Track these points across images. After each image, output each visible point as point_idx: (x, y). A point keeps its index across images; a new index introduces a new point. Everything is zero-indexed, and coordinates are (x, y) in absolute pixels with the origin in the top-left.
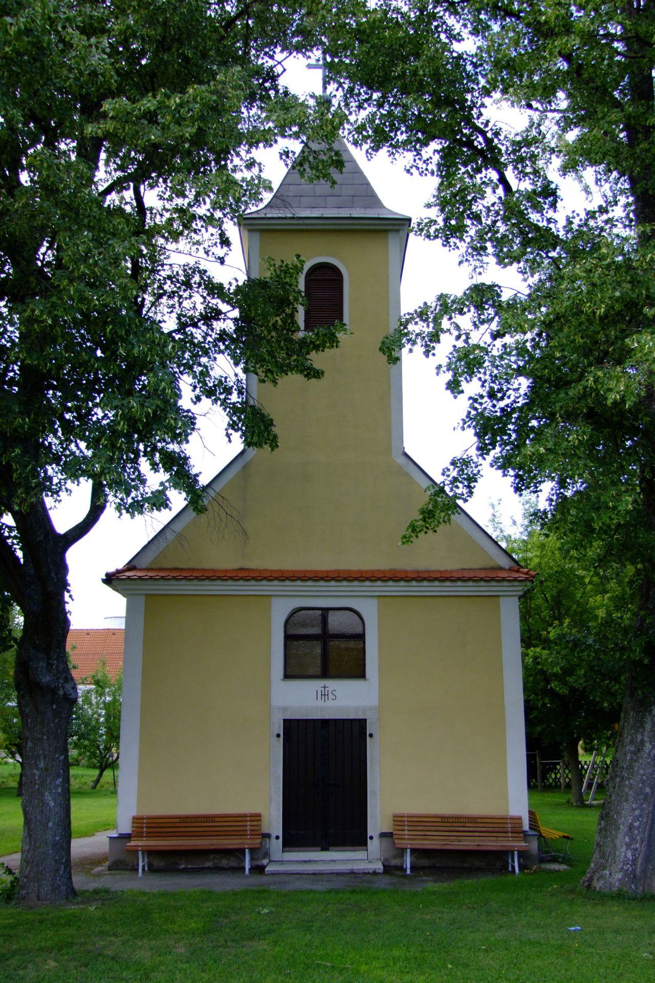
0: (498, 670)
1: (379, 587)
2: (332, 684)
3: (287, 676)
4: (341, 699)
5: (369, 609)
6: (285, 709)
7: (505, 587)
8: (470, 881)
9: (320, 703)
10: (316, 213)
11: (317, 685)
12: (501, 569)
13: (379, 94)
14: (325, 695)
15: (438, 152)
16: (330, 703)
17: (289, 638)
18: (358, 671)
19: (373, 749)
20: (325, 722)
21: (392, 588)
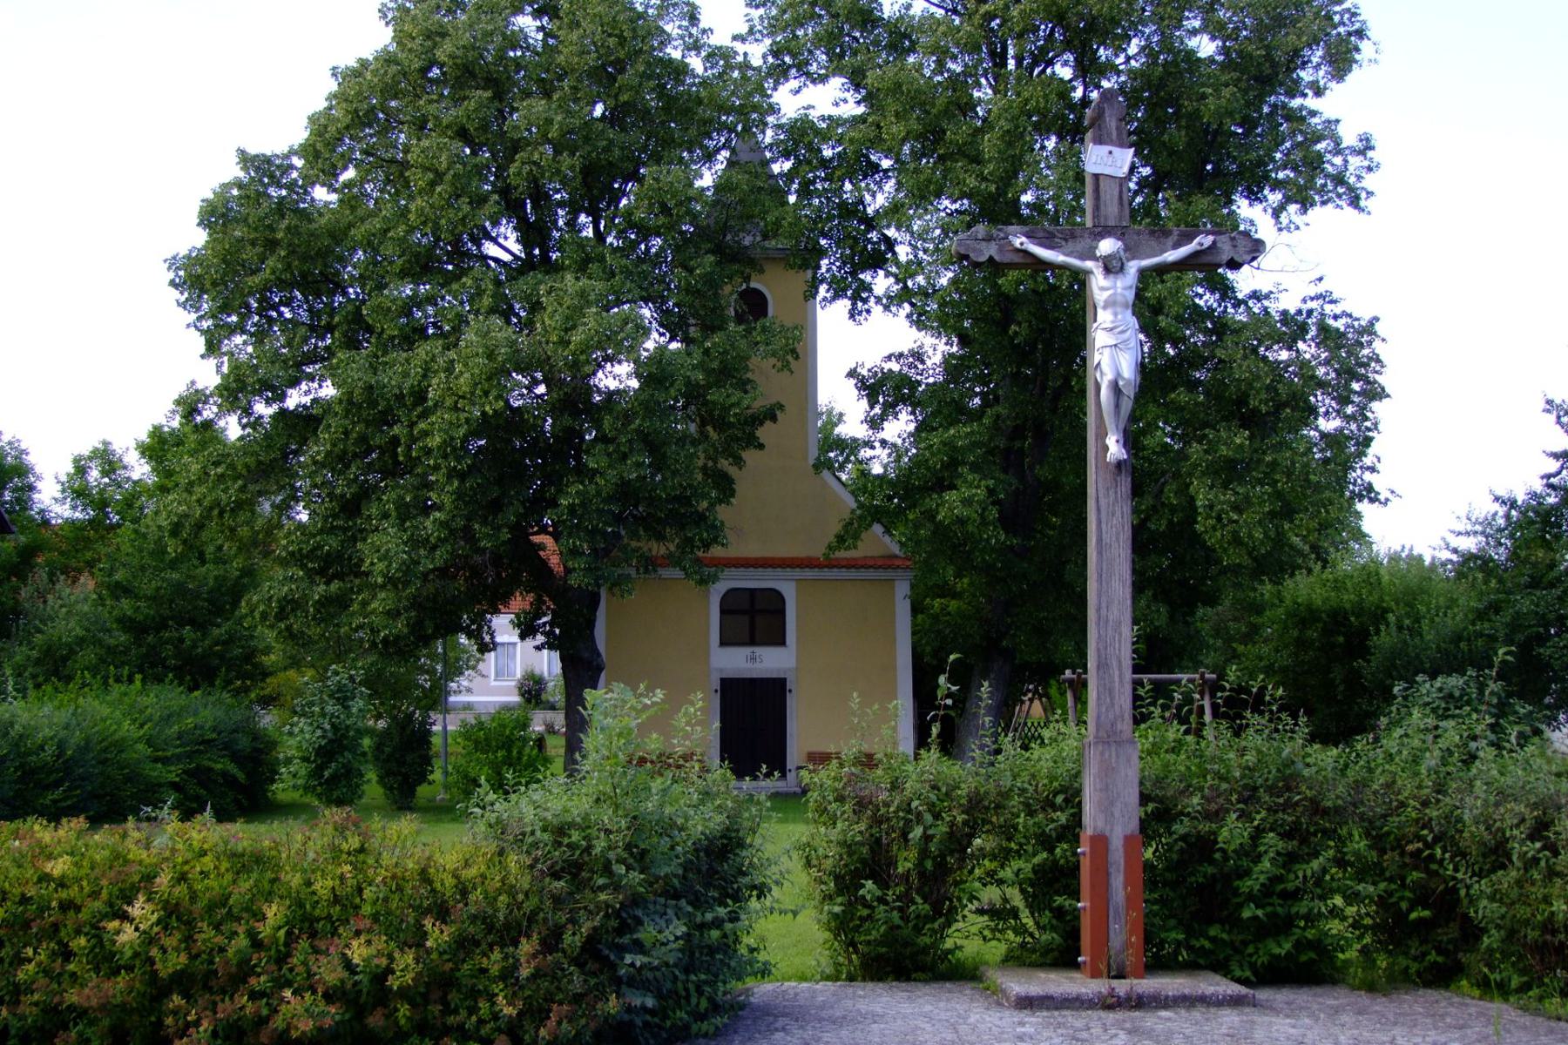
0: (893, 641)
1: (798, 573)
2: (759, 650)
3: (723, 643)
4: (768, 661)
5: (788, 590)
6: (721, 670)
7: (900, 572)
8: (906, 1008)
9: (749, 665)
10: (1091, 491)
11: (747, 651)
12: (896, 557)
13: (698, 184)
14: (753, 659)
15: (1268, 57)
16: (757, 665)
17: (722, 612)
18: (780, 641)
19: (792, 703)
20: (753, 681)
21: (809, 574)
